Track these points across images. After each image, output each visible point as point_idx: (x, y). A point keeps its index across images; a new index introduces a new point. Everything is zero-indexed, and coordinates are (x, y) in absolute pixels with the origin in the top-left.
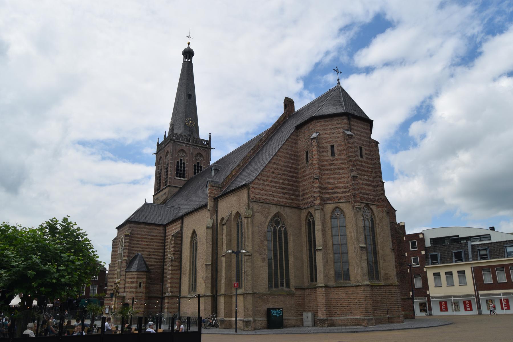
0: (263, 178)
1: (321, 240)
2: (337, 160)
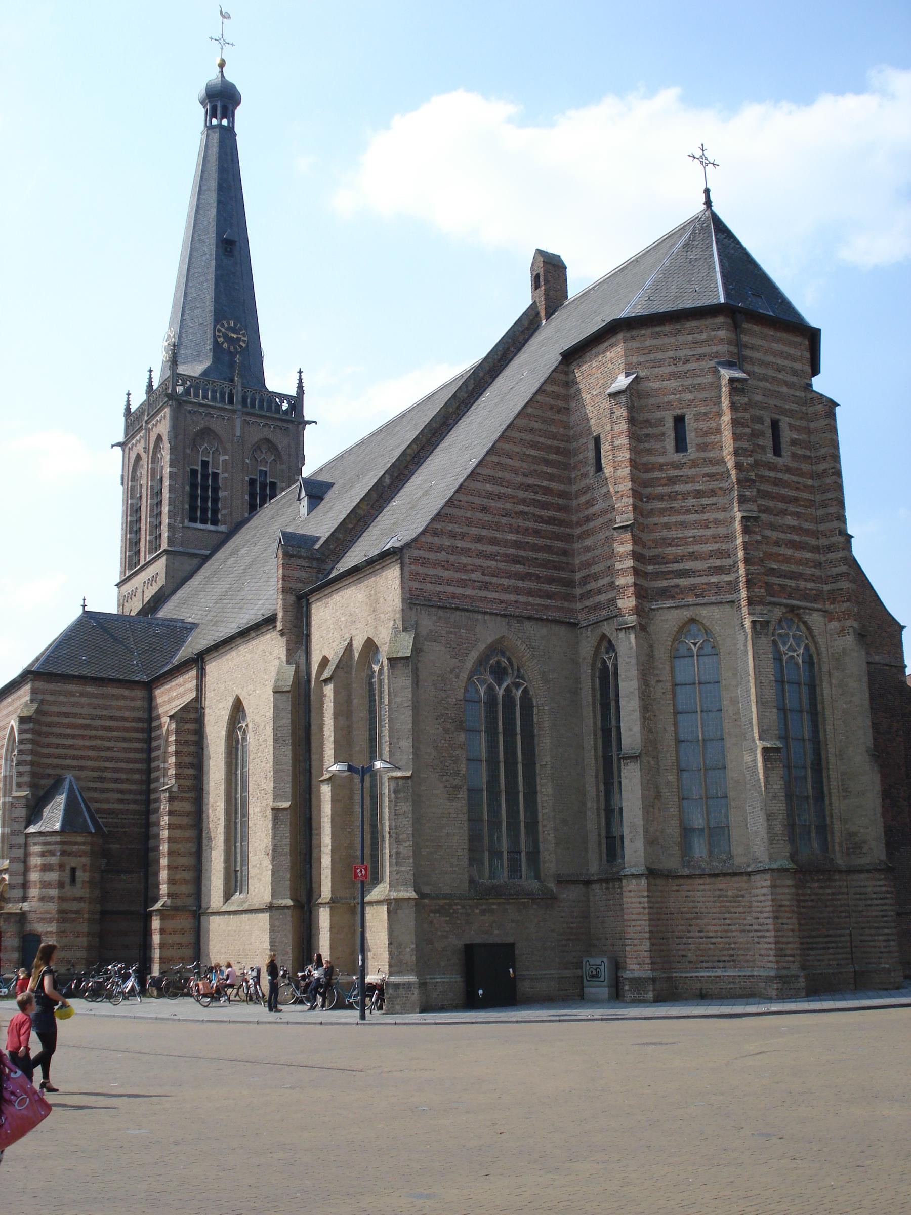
0: (450, 527)
1: (637, 728)
2: (694, 464)
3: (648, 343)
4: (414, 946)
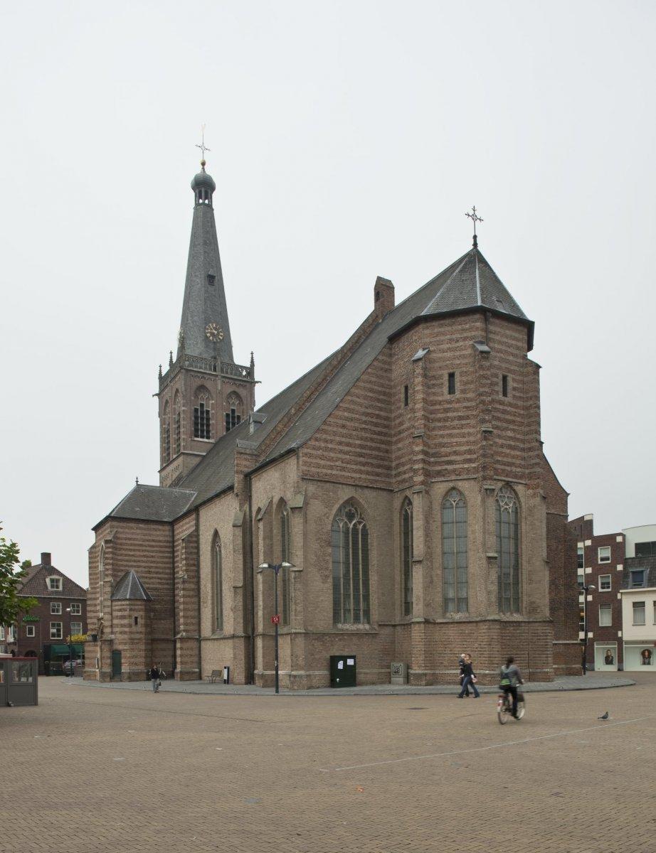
0: (324, 436)
1: (421, 546)
2: (458, 401)
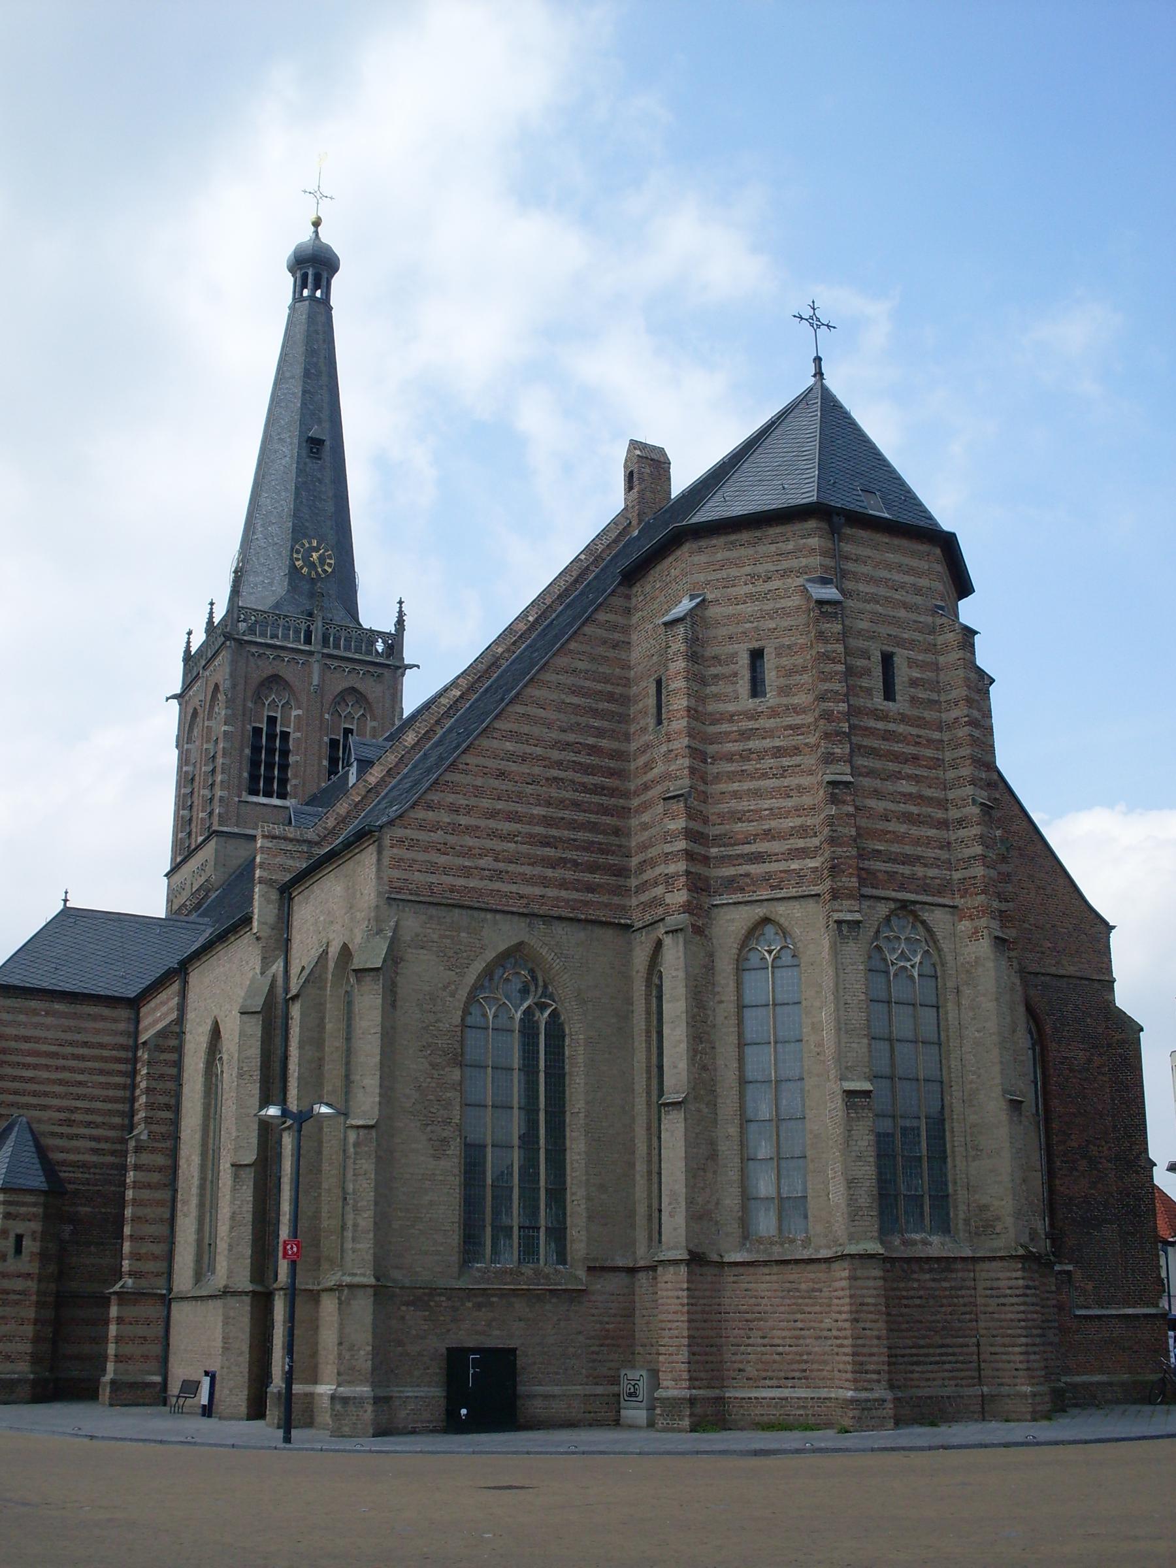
0: (451, 798)
1: (683, 1065)
2: (774, 713)
3: (719, 556)
4: (370, 1348)
